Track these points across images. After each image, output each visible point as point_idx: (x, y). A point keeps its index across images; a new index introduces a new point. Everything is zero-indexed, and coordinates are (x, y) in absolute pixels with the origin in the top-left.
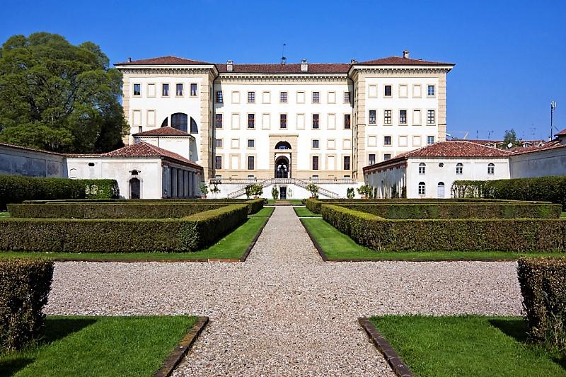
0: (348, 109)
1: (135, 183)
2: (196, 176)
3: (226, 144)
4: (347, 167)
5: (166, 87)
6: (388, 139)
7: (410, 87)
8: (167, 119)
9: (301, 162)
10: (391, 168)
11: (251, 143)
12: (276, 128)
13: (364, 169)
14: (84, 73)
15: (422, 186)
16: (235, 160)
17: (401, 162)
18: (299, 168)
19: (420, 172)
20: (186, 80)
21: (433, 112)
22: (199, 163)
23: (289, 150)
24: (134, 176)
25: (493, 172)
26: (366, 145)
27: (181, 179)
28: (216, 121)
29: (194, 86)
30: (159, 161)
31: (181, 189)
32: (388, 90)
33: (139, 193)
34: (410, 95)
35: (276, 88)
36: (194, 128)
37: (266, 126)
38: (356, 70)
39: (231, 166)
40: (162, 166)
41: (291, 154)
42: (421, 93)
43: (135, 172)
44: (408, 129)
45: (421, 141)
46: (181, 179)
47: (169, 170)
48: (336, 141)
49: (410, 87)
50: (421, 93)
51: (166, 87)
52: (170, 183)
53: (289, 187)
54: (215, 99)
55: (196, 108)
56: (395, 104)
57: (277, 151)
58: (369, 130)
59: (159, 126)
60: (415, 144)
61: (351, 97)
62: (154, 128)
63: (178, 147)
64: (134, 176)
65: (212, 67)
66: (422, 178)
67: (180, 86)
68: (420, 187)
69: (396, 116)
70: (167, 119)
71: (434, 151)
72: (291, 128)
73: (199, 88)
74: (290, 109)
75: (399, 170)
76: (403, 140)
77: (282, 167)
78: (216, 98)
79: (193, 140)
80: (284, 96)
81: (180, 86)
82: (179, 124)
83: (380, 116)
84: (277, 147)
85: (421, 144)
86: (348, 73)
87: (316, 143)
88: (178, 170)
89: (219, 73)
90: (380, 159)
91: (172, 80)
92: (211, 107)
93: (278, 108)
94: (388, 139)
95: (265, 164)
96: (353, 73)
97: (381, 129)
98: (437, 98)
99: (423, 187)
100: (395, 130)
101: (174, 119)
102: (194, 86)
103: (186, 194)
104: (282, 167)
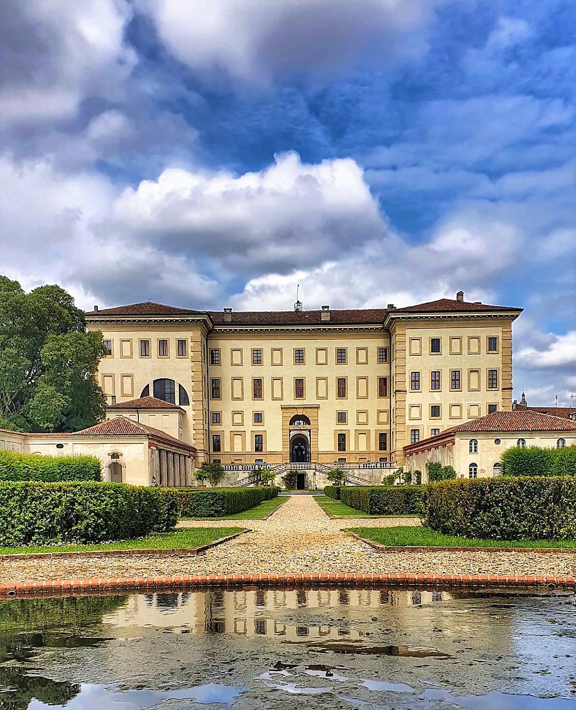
0: (382, 370)
1: (116, 468)
2: (189, 460)
3: (226, 418)
4: (383, 445)
5: (145, 344)
6: (435, 411)
7: (465, 341)
8: (148, 386)
9: (323, 442)
10: (436, 447)
11: (258, 418)
12: (290, 399)
13: (405, 449)
14: (318, 691)
15: (473, 468)
16: (238, 440)
17: (447, 439)
18: (321, 449)
19: (471, 451)
20: (173, 337)
21: (494, 373)
22: (192, 443)
23: (308, 427)
24: (114, 460)
25: (475, 451)
26: (407, 418)
27: (171, 464)
28: (214, 389)
29: (182, 343)
30: (146, 442)
31: (171, 477)
32: (435, 346)
33: (254, 313)
34: (465, 351)
35: (289, 346)
36: (184, 400)
37: (277, 394)
38: (392, 319)
39: (232, 447)
40: (149, 448)
41: (310, 432)
42: (479, 347)
43: (115, 456)
44: (463, 397)
45: (479, 409)
46: (171, 464)
47: (157, 452)
48: (365, 411)
49: (465, 341)
50: (479, 347)
51: (145, 344)
52: (158, 470)
53: (310, 473)
54: (210, 359)
55: (183, 371)
56: (444, 363)
57: (292, 427)
58: (411, 398)
59: (137, 396)
60: (472, 414)
61: (385, 355)
62: (131, 399)
63: (165, 423)
64: (114, 460)
65: (205, 317)
66: (473, 458)
67: (163, 344)
68: (471, 470)
69: (446, 380)
70: (148, 386)
71: (477, 429)
72: (310, 398)
73: (190, 344)
74: (308, 371)
75: (446, 449)
76: (456, 412)
77: (300, 449)
78: (212, 357)
79: (183, 413)
80: (299, 356)
81: (163, 344)
82: (163, 394)
83: (426, 381)
84: (292, 422)
85: (479, 414)
86: (383, 323)
87: (342, 417)
88: (167, 452)
89: (214, 325)
90: (425, 435)
91: (154, 336)
92: (205, 370)
93: (290, 372)
94: (435, 411)
95: (277, 442)
96: (390, 324)
97: (426, 397)
98: (500, 353)
99: (475, 469)
100: (444, 397)
101: (157, 386)
102: (182, 343)
103: (177, 483)
104: (300, 449)
